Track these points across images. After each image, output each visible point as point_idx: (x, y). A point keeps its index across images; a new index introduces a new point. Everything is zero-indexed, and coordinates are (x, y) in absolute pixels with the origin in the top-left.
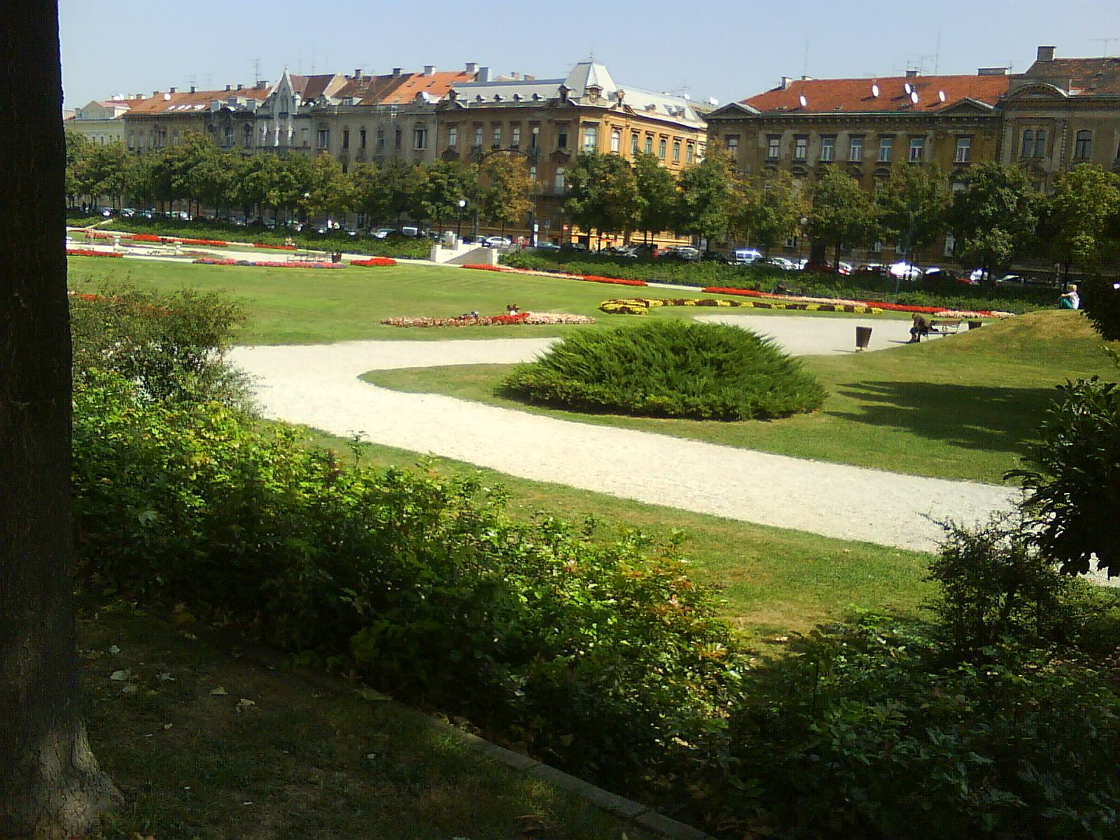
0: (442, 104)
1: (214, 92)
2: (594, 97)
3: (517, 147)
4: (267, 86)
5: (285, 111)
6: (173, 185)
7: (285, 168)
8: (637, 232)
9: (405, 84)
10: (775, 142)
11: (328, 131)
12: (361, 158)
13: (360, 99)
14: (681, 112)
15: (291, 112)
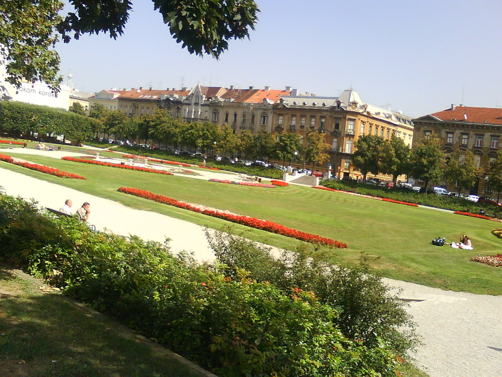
1: (161, 91)
2: (354, 107)
3: (313, 127)
5: (197, 102)
6: (149, 133)
7: (205, 129)
8: (370, 172)
9: (255, 94)
10: (450, 135)
11: (218, 113)
13: (234, 100)
14: (390, 117)
15: (200, 103)
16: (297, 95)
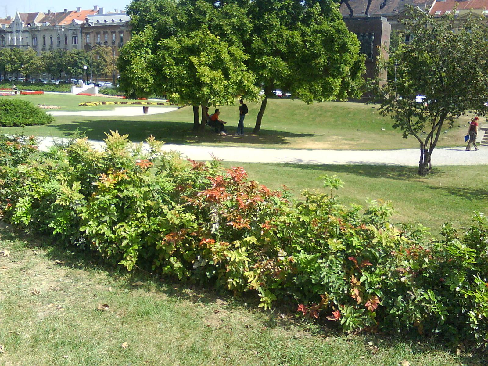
0: (84, 24)
4: (11, 19)
9: (69, 16)
12: (44, 49)
16: (104, 13)
